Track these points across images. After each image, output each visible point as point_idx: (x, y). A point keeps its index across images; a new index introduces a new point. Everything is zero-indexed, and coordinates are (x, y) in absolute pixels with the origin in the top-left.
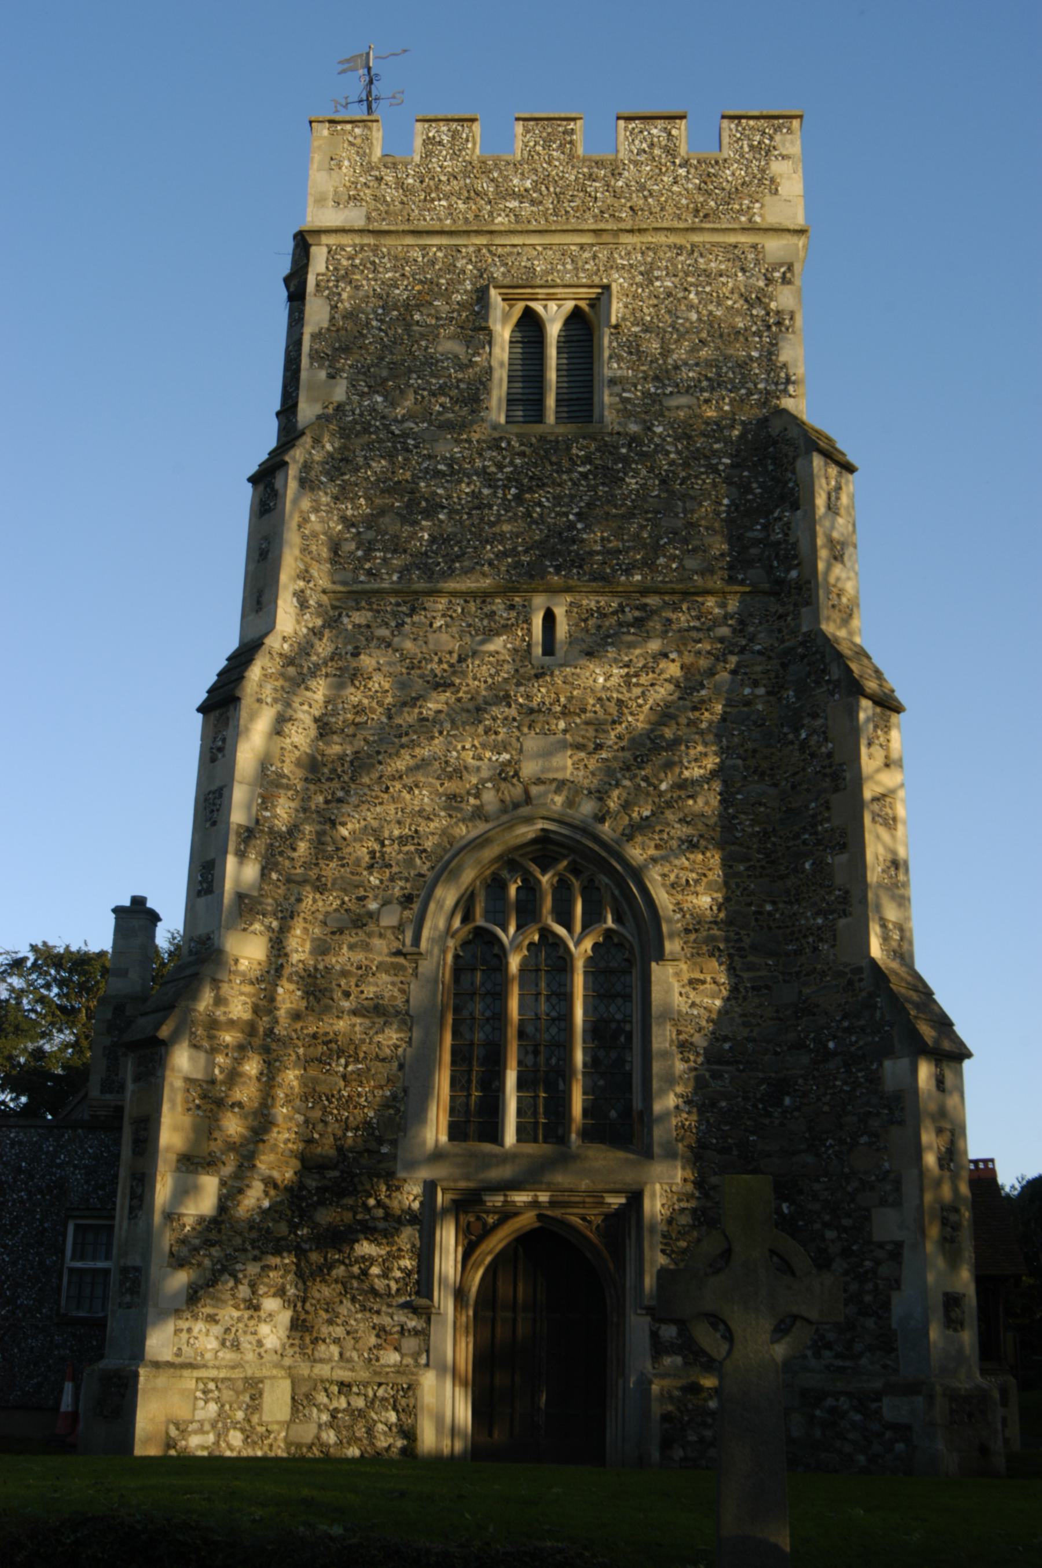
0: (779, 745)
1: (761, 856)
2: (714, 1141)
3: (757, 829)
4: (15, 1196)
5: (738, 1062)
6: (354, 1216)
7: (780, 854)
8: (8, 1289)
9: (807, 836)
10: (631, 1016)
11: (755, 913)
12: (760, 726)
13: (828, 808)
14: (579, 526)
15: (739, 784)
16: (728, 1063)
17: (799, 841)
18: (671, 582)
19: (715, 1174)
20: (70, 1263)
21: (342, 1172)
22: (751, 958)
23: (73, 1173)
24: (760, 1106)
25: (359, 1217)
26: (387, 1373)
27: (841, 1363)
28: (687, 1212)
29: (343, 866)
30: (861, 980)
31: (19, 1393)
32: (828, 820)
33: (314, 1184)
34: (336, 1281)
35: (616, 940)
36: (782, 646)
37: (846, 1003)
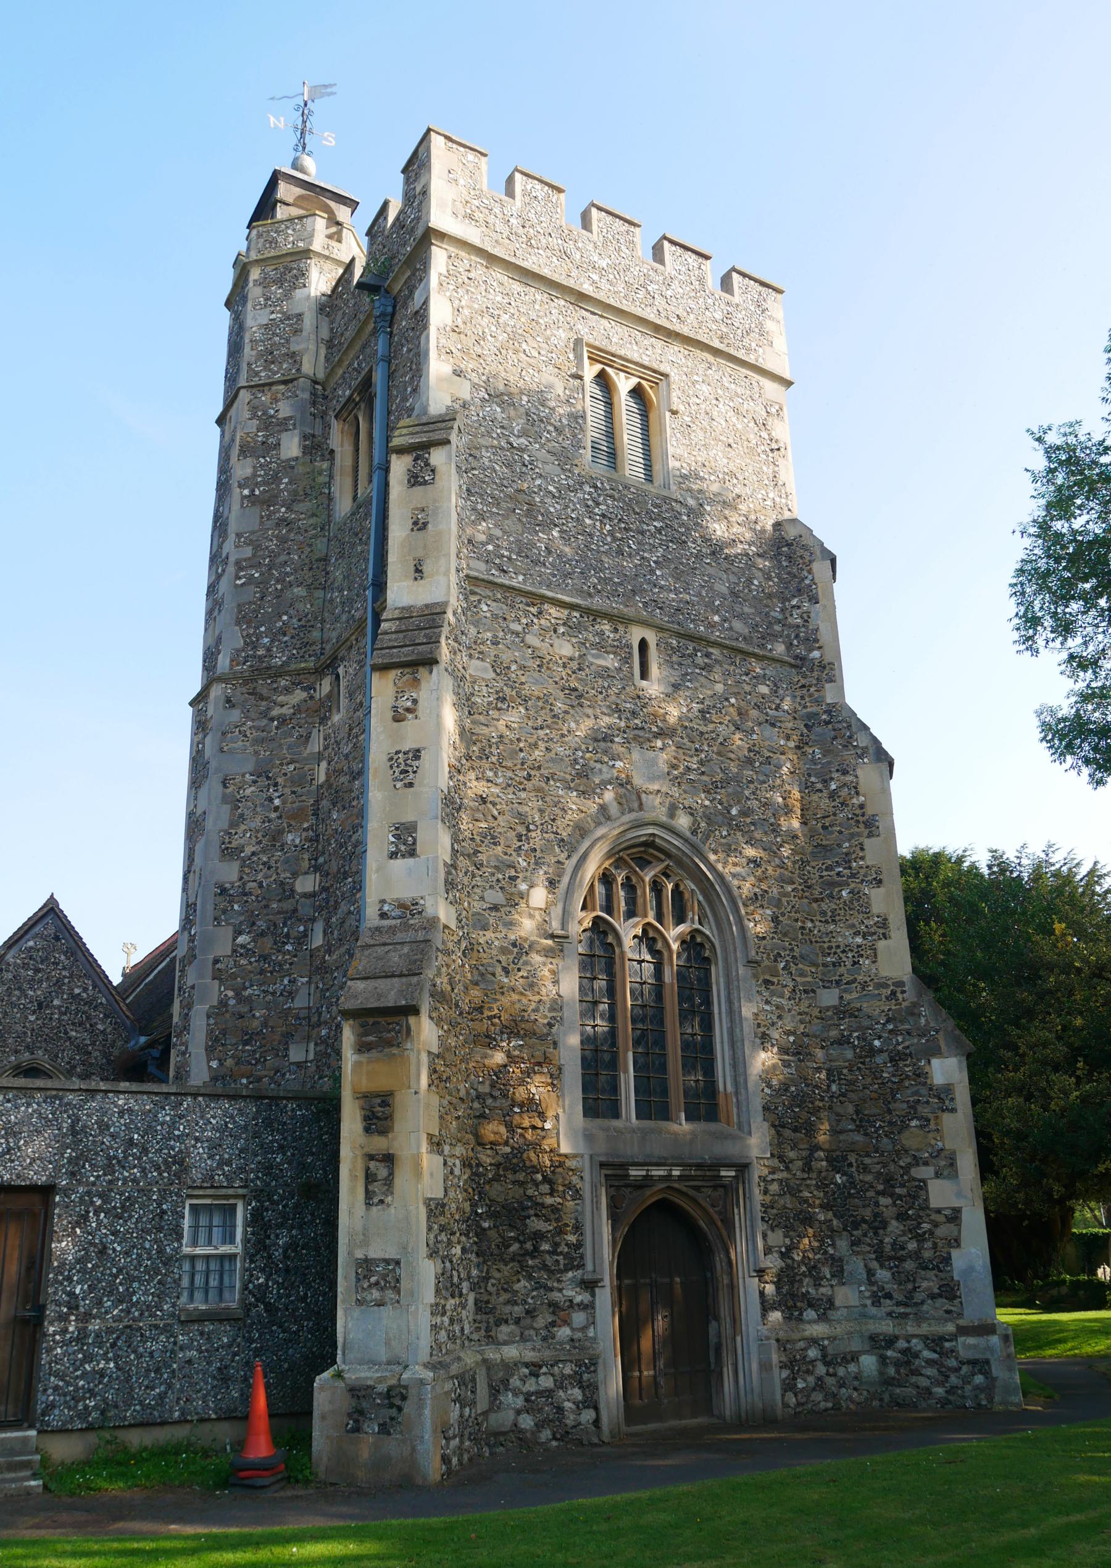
4: (126, 1174)
8: (121, 1284)
13: (862, 849)
14: (658, 573)
18: (725, 638)
20: (187, 1250)
23: (194, 1146)
27: (902, 1310)
30: (903, 992)
31: (138, 1408)
32: (862, 858)
33: (488, 1161)
34: (513, 1260)
36: (805, 711)
37: (889, 1010)
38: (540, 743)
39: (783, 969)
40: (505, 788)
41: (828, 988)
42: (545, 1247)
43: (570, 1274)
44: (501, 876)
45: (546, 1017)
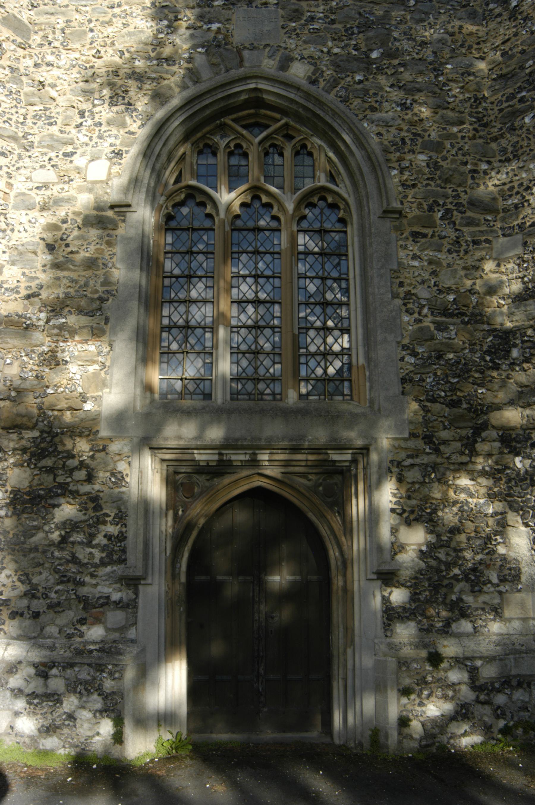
0: (484, 23)
1: (474, 120)
2: (443, 394)
3: (467, 95)
5: (463, 314)
6: (55, 479)
7: (492, 118)
9: (524, 94)
10: (347, 274)
11: (470, 171)
12: (464, 6)
15: (448, 56)
16: (452, 315)
17: (515, 101)
19: (445, 428)
21: (42, 432)
22: (469, 214)
24: (488, 358)
25: (60, 479)
26: (91, 651)
28: (417, 468)
29: (51, 124)
35: (330, 200)
38: (114, 20)
39: (441, 218)
40: (68, 69)
41: (510, 235)
42: (77, 537)
43: (109, 569)
44: (53, 155)
45: (97, 291)
